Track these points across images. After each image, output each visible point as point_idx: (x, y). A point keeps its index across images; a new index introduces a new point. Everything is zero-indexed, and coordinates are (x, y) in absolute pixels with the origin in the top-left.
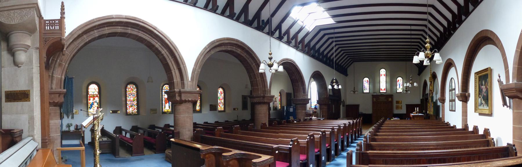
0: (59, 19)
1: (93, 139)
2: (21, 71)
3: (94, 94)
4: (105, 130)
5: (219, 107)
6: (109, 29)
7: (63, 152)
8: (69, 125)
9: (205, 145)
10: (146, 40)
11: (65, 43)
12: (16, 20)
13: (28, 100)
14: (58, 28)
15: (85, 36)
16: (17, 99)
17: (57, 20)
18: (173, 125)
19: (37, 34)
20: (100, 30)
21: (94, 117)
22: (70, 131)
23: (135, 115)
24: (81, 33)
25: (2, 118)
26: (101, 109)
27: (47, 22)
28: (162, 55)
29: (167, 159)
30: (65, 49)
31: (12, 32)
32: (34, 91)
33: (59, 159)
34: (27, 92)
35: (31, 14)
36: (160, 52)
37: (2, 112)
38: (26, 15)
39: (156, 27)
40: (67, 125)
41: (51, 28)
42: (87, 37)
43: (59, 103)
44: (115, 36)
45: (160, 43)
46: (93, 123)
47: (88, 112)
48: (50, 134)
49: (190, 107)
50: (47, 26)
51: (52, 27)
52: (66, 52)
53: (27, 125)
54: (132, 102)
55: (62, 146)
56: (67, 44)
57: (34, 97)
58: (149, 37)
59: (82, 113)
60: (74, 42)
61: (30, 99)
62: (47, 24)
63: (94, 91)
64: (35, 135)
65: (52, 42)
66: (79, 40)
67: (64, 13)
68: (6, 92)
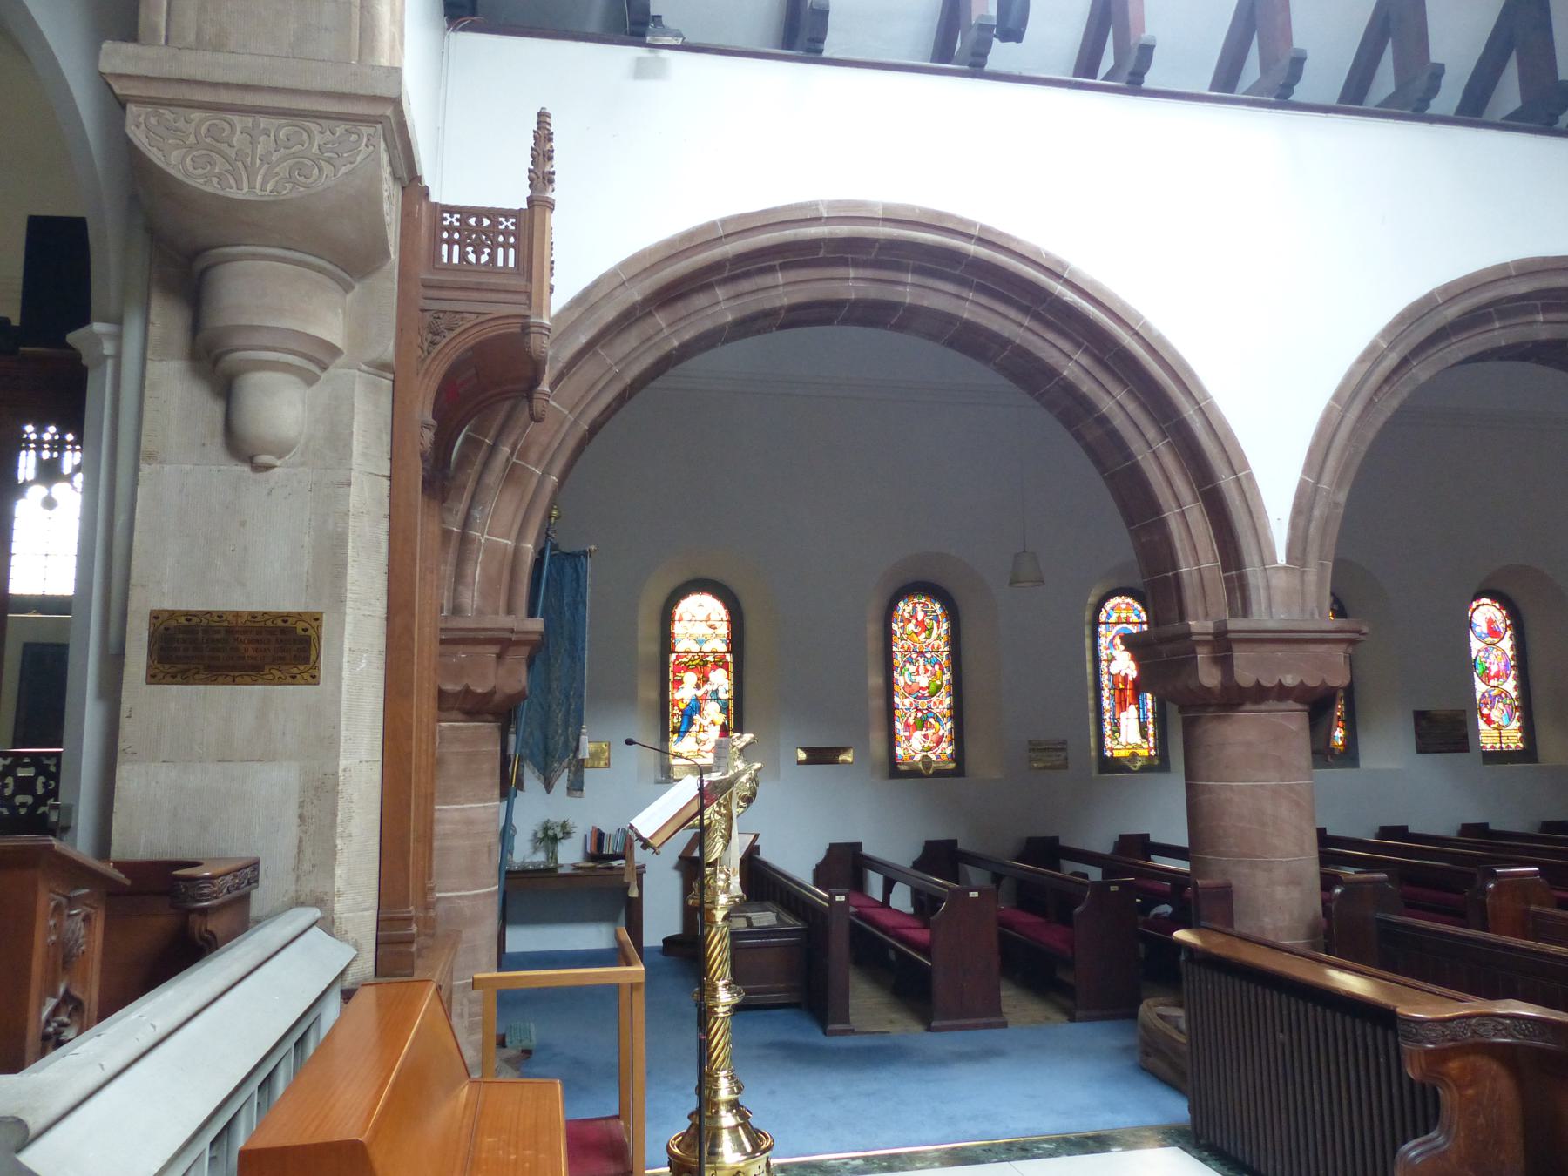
0: (516, 207)
1: (696, 914)
2: (269, 493)
3: (707, 648)
4: (765, 864)
5: (1482, 725)
6: (795, 283)
7: (509, 1001)
8: (550, 833)
9: (1430, 987)
10: (1005, 342)
11: (550, 353)
12: (259, 178)
13: (306, 676)
14: (511, 263)
15: (660, 319)
16: (233, 668)
17: (507, 214)
18: (1183, 841)
19: (387, 282)
20: (745, 285)
21: (702, 781)
22: (554, 870)
23: (940, 773)
24: (638, 298)
25: (118, 784)
26: (748, 737)
27: (451, 220)
28: (1103, 420)
29: (1151, 1060)
30: (545, 387)
31: (227, 246)
32: (349, 619)
33: (484, 1044)
34: (300, 626)
35: (359, 159)
36: (1085, 405)
37: (121, 745)
38: (329, 161)
39: (1060, 263)
40: (540, 835)
41: (472, 258)
42: (670, 325)
43: (497, 697)
44: (827, 321)
45: (1086, 351)
46: (696, 821)
47: (664, 752)
48: (432, 889)
49: (1294, 727)
50: (450, 242)
51: (478, 253)
52: (552, 403)
53: (291, 831)
54: (922, 697)
55: (504, 960)
56: (556, 355)
57: (345, 659)
58: (1021, 325)
59: (638, 762)
60: (597, 348)
61: (316, 666)
62: (450, 229)
63: (702, 630)
64: (340, 893)
65: (472, 339)
66: (631, 340)
67: (549, 179)
68: (155, 616)
